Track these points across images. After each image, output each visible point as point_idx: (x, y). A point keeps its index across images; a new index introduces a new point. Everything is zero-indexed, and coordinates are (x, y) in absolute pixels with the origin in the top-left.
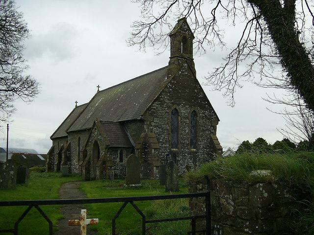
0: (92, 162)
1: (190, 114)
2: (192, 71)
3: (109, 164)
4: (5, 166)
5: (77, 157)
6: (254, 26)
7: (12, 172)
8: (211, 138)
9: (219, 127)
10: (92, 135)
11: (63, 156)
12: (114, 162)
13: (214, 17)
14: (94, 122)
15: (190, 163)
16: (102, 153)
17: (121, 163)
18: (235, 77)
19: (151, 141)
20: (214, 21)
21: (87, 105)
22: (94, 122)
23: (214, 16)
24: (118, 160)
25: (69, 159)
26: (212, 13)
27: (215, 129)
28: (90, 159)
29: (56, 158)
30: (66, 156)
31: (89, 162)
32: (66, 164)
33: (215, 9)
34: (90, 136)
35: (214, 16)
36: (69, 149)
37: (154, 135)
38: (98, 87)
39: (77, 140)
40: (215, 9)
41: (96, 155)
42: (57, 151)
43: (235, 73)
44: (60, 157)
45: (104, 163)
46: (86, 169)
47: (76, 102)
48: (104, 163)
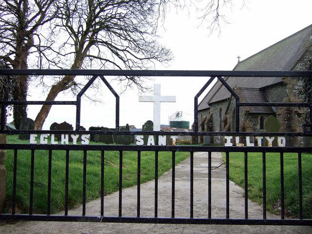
11: (206, 127)
24: (258, 126)
30: (208, 127)
36: (211, 120)
38: (239, 58)
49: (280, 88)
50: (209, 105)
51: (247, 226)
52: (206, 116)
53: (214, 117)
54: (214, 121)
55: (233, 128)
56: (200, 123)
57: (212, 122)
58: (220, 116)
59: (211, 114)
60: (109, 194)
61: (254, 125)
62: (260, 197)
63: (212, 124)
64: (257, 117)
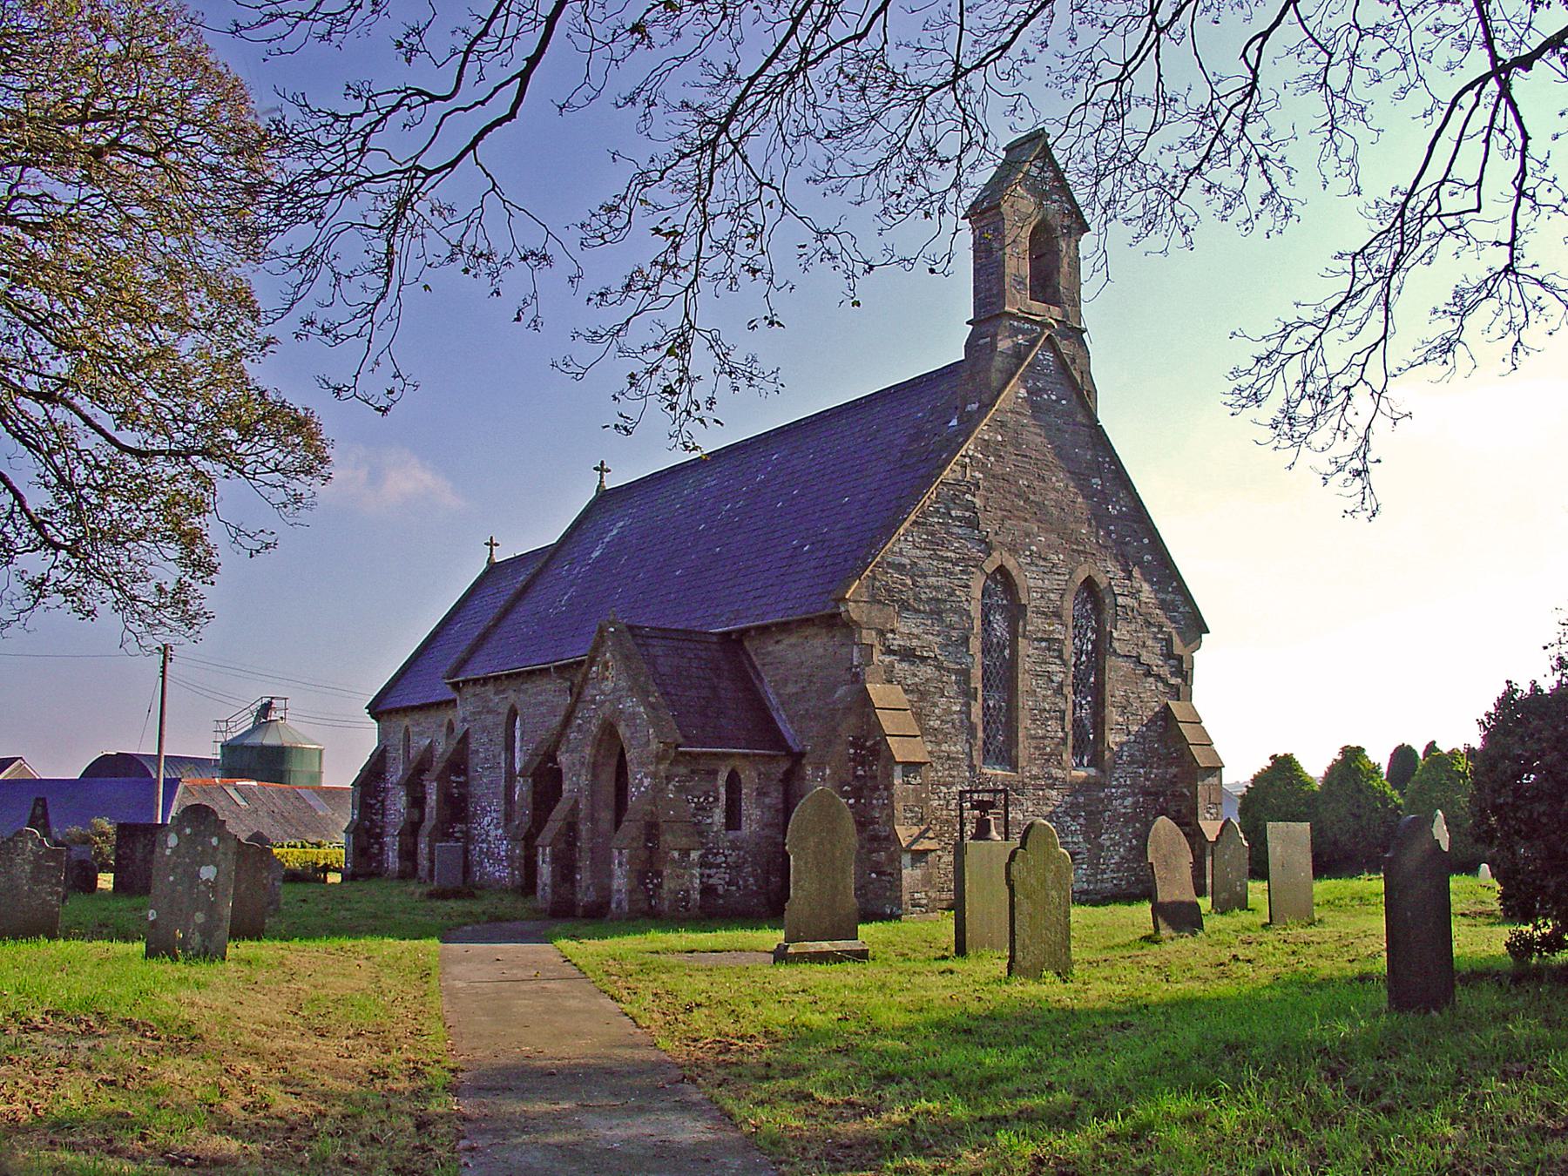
0: (584, 828)
1: (1069, 598)
2: (1080, 393)
3: (671, 840)
4: (173, 840)
5: (498, 804)
6: (1482, 117)
7: (208, 872)
8: (1166, 714)
9: (1206, 661)
10: (590, 692)
11: (432, 798)
12: (700, 831)
13: (1255, 79)
14: (431, 895)
15: (1074, 833)
16: (640, 781)
17: (732, 835)
18: (1374, 374)
19: (888, 727)
20: (1250, 94)
21: (548, 556)
22: (431, 895)
23: (1254, 72)
24: (719, 816)
25: (457, 808)
26: (1244, 55)
27: (1184, 672)
28: (574, 809)
29: (398, 803)
30: (446, 798)
31: (571, 827)
32: (447, 836)
33: (1265, 35)
34: (577, 695)
35: (1254, 72)
36: (459, 763)
37: (902, 699)
38: (601, 469)
39: (503, 718)
40: (1265, 35)
41: (608, 789)
42: (396, 773)
43: (1377, 355)
44: (417, 802)
45: (652, 830)
46: (555, 859)
47: (491, 544)
48: (652, 830)
49: (817, 642)
50: (455, 686)
51: (966, 309)
52: (430, 735)
53: (473, 746)
54: (477, 763)
55: (593, 820)
56: (396, 773)
57: (465, 772)
58: (509, 748)
59: (459, 732)
60: (631, 1156)
61: (700, 807)
62: (1497, 243)
63: (464, 785)
64: (714, 773)
